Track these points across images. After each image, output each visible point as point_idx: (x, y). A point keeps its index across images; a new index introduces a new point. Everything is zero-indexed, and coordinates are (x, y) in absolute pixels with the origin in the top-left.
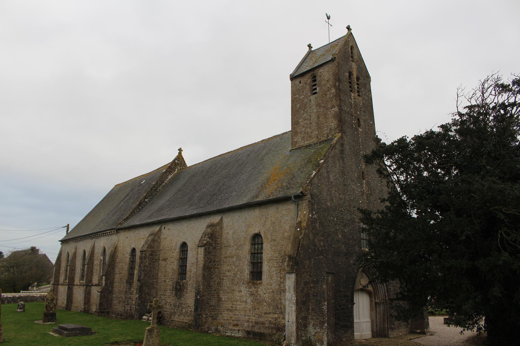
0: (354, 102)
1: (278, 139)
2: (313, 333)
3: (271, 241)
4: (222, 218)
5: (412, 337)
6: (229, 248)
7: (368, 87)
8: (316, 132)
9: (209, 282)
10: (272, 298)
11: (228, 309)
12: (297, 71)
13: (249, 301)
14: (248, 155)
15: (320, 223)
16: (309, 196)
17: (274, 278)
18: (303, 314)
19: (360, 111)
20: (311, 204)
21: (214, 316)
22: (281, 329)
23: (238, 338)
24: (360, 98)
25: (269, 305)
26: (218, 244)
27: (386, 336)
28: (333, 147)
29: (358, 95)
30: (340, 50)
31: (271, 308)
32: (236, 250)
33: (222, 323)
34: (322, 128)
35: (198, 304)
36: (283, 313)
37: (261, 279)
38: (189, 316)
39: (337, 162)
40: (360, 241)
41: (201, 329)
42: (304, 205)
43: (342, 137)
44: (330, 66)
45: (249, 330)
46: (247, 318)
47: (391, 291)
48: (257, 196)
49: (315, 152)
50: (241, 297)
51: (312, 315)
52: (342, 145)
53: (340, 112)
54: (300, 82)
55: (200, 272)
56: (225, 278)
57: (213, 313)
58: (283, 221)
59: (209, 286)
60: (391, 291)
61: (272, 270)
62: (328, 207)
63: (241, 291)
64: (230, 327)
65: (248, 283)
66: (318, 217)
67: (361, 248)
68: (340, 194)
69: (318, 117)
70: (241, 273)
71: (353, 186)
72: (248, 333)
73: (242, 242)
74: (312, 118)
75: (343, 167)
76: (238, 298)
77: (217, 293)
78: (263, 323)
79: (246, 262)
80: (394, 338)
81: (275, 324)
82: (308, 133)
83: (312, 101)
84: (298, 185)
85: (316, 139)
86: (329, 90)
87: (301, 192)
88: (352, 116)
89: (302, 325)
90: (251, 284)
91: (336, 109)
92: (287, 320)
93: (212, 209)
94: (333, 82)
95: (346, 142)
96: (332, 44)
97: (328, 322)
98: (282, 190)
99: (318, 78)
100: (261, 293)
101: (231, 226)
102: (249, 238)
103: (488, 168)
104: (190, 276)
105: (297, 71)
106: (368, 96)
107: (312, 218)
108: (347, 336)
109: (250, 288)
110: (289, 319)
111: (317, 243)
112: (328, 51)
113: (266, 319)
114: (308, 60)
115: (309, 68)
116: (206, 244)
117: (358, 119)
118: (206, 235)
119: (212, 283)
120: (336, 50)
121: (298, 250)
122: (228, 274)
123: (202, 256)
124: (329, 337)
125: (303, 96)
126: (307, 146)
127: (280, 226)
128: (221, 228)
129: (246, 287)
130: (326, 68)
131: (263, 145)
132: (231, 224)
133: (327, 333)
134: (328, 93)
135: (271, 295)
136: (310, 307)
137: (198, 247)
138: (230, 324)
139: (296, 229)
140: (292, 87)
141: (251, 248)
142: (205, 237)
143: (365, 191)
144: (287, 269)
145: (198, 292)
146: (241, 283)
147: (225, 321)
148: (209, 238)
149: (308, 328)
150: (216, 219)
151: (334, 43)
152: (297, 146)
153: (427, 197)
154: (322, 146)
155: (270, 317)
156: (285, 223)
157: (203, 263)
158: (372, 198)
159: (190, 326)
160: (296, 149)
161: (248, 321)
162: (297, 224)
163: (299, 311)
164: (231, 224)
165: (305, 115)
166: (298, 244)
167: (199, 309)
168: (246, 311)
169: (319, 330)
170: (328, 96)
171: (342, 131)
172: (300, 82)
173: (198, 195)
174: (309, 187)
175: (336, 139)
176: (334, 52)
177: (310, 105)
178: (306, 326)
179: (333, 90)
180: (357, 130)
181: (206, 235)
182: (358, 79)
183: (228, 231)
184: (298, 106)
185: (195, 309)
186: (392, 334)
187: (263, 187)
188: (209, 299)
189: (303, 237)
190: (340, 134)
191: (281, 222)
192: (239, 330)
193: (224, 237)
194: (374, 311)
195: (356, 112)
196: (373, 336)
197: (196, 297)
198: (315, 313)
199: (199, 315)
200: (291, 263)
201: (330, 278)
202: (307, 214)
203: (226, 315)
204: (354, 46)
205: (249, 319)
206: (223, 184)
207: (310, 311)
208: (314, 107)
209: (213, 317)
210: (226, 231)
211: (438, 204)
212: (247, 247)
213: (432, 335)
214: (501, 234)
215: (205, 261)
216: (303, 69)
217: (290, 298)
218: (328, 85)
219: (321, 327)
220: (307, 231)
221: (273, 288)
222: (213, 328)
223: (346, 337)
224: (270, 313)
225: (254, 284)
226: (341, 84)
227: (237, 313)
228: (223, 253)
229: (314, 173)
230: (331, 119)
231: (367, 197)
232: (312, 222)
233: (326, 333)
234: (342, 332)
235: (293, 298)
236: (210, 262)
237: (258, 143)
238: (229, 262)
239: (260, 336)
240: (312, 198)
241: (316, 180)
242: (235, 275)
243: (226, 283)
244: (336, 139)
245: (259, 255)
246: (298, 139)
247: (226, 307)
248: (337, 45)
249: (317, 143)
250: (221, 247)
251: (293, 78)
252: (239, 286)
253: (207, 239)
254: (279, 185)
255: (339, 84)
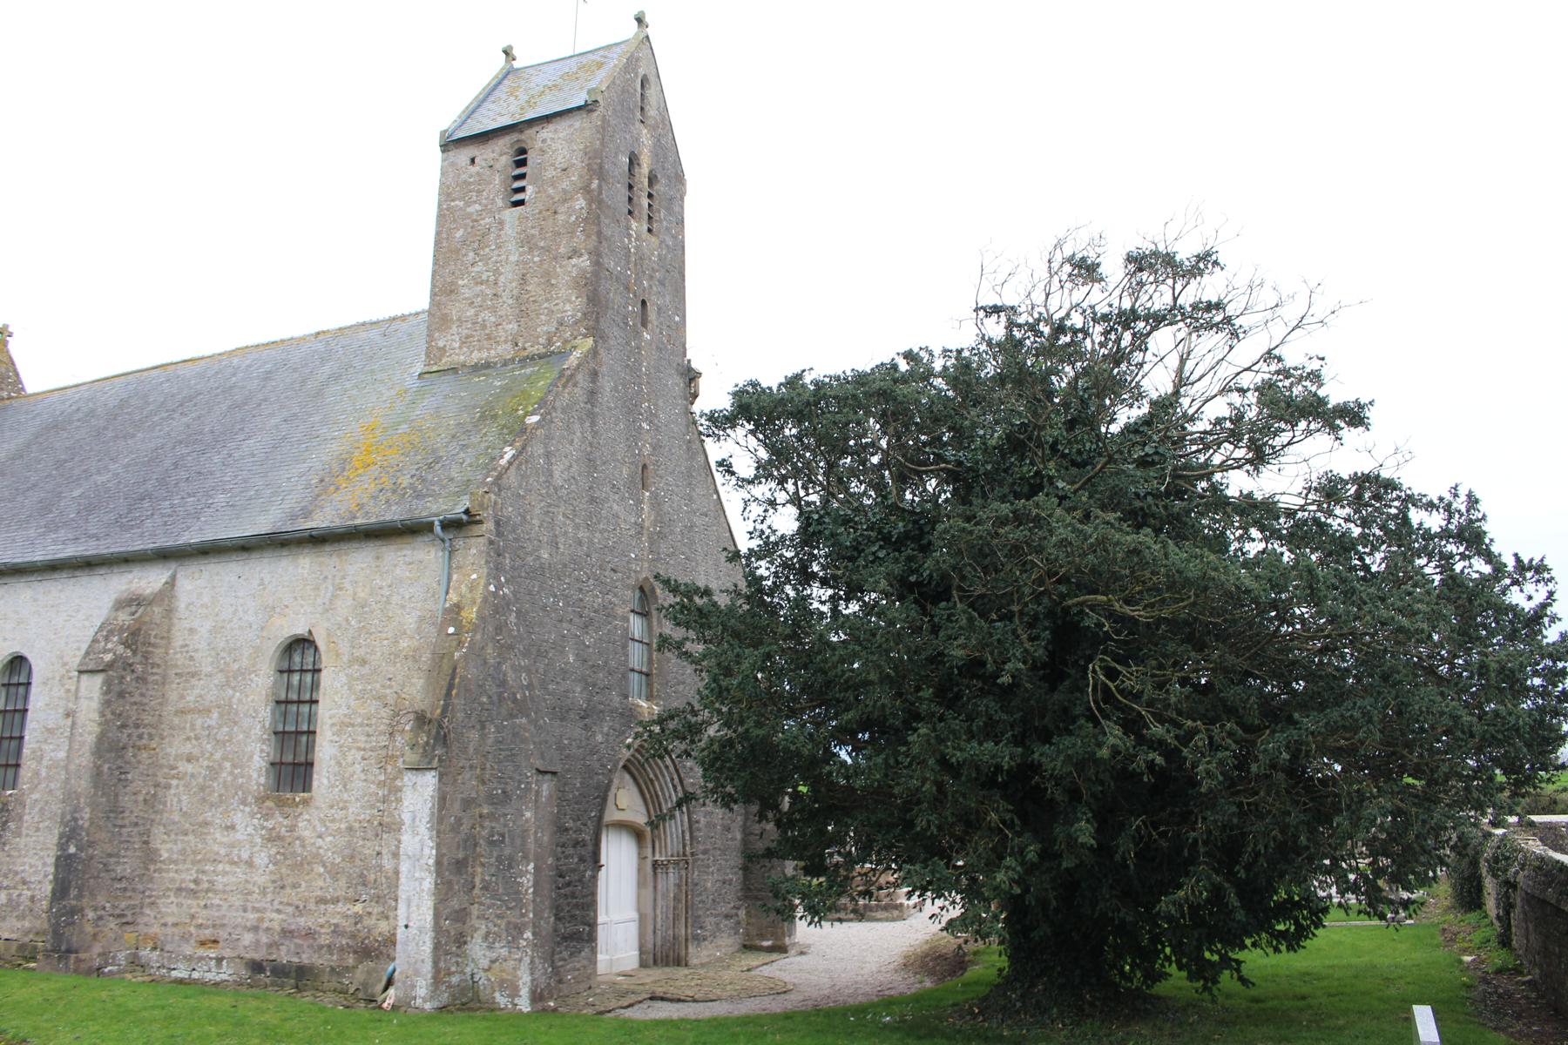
0: (637, 248)
1: (374, 334)
2: (485, 963)
3: (351, 663)
4: (173, 578)
5: (752, 960)
6: (194, 681)
7: (677, 209)
8: (513, 326)
9: (116, 795)
10: (347, 852)
11: (180, 889)
12: (464, 123)
13: (261, 859)
14: (267, 376)
15: (519, 612)
16: (489, 525)
17: (357, 784)
18: (455, 904)
19: (651, 277)
20: (496, 552)
21: (128, 913)
22: (376, 950)
23: (216, 984)
24: (653, 239)
25: (334, 873)
26: (153, 665)
27: (679, 961)
28: (567, 378)
29: (650, 230)
30: (613, 83)
31: (342, 883)
32: (222, 687)
33: (154, 938)
34: (533, 315)
35: (70, 874)
36: (386, 896)
37: (307, 787)
38: (22, 917)
39: (577, 426)
40: (624, 677)
41: (78, 960)
42: (473, 551)
43: (594, 352)
44: (577, 125)
45: (257, 956)
46: (252, 916)
47: (699, 830)
48: (307, 514)
49: (506, 389)
50: (232, 846)
51: (481, 904)
52: (594, 375)
53: (596, 274)
54: (473, 161)
55: (85, 759)
56: (174, 782)
57: (123, 904)
58: (395, 599)
59: (115, 810)
60: (699, 830)
61: (350, 759)
62: (542, 567)
63: (233, 827)
64: (188, 950)
65: (261, 800)
66: (514, 593)
67: (626, 697)
68: (577, 527)
69: (523, 279)
70: (234, 766)
71: (615, 507)
72: (256, 967)
73: (245, 662)
74: (502, 279)
75: (591, 444)
76: (223, 852)
77: (141, 835)
78: (310, 934)
79: (257, 731)
80: (703, 965)
81: (353, 936)
82: (484, 327)
83: (507, 227)
84: (452, 488)
85: (509, 346)
86: (565, 200)
87: (467, 512)
88: (627, 288)
89: (450, 938)
90: (269, 804)
91: (584, 262)
92: (402, 923)
93: (138, 546)
94: (581, 176)
95: (604, 369)
96: (584, 60)
97: (534, 926)
98: (394, 498)
99: (532, 157)
100: (307, 833)
101: (204, 606)
102: (272, 648)
103: (1061, 484)
104: (37, 773)
105: (464, 123)
106: (675, 237)
107: (495, 594)
108: (578, 965)
109: (266, 817)
110: (408, 918)
111: (511, 676)
112: (569, 77)
113: (322, 921)
114: (501, 93)
115: (506, 121)
116: (110, 666)
117: (644, 302)
118: (111, 632)
119: (125, 800)
120: (599, 80)
121: (448, 694)
122: (184, 767)
123: (95, 705)
124: (537, 974)
125: (477, 207)
126: (477, 368)
127: (386, 618)
128: (170, 612)
129: (252, 815)
130: (562, 128)
131: (321, 347)
132: (206, 599)
133: (532, 962)
134: (562, 209)
135: (342, 841)
136: (477, 880)
137: (80, 672)
138: (185, 938)
139: (442, 629)
140: (443, 173)
141: (275, 683)
142: (107, 639)
143: (647, 524)
144: (412, 757)
145: (73, 830)
146: (235, 802)
147: (169, 930)
148: (126, 644)
149: (468, 946)
150: (150, 580)
151: (590, 57)
152: (445, 362)
153: (881, 554)
154: (528, 371)
155: (338, 914)
156: (403, 607)
157: (97, 729)
158: (663, 548)
159: (28, 953)
160: (439, 371)
161: (255, 929)
162: (446, 611)
163: (443, 891)
164: (206, 599)
165: (480, 267)
166: (449, 682)
167: (73, 892)
168: (250, 893)
169: (504, 952)
170: (561, 217)
171: (595, 332)
172: (473, 161)
173: (76, 493)
174: (493, 497)
175: (577, 354)
176: (592, 85)
177: (499, 236)
178: (461, 940)
179: (580, 203)
180: (638, 335)
181: (111, 632)
182: (652, 180)
183: (195, 624)
184: (459, 234)
185: (54, 891)
186: (697, 954)
187: (326, 484)
188: (110, 855)
189: (465, 656)
190: (590, 341)
191: (388, 602)
192: (219, 960)
193: (178, 642)
194: (651, 888)
195: (638, 280)
196: (643, 964)
197: (62, 846)
198: (492, 897)
199: (73, 911)
200: (423, 739)
201: (545, 786)
202: (482, 582)
203: (172, 908)
204: (652, 79)
205: (261, 920)
206: (176, 465)
207: (476, 891)
208: (512, 246)
209: (123, 916)
210: (186, 624)
211: (913, 579)
212: (263, 681)
213: (802, 953)
214: (1094, 671)
215: (105, 724)
216: (485, 121)
217: (417, 846)
218: (565, 185)
219: (513, 943)
220: (478, 637)
221: (351, 818)
222: (121, 956)
223: (575, 969)
224: (336, 901)
225: (281, 804)
226: (605, 187)
227: (217, 901)
228: (173, 696)
229: (509, 452)
230: (563, 292)
231: (651, 544)
232: (496, 607)
233: (527, 960)
234: (565, 954)
235: (427, 851)
236: (124, 726)
237: (303, 338)
238: (193, 728)
239: (300, 977)
240: (499, 534)
241: (512, 478)
242: (214, 772)
243: (178, 799)
244: (577, 354)
245: (305, 708)
246: (450, 340)
247: (172, 880)
248: (600, 65)
249: (513, 360)
250: (164, 677)
251: (450, 144)
252: (226, 811)
253: (114, 648)
254: (387, 482)
255: (600, 186)
